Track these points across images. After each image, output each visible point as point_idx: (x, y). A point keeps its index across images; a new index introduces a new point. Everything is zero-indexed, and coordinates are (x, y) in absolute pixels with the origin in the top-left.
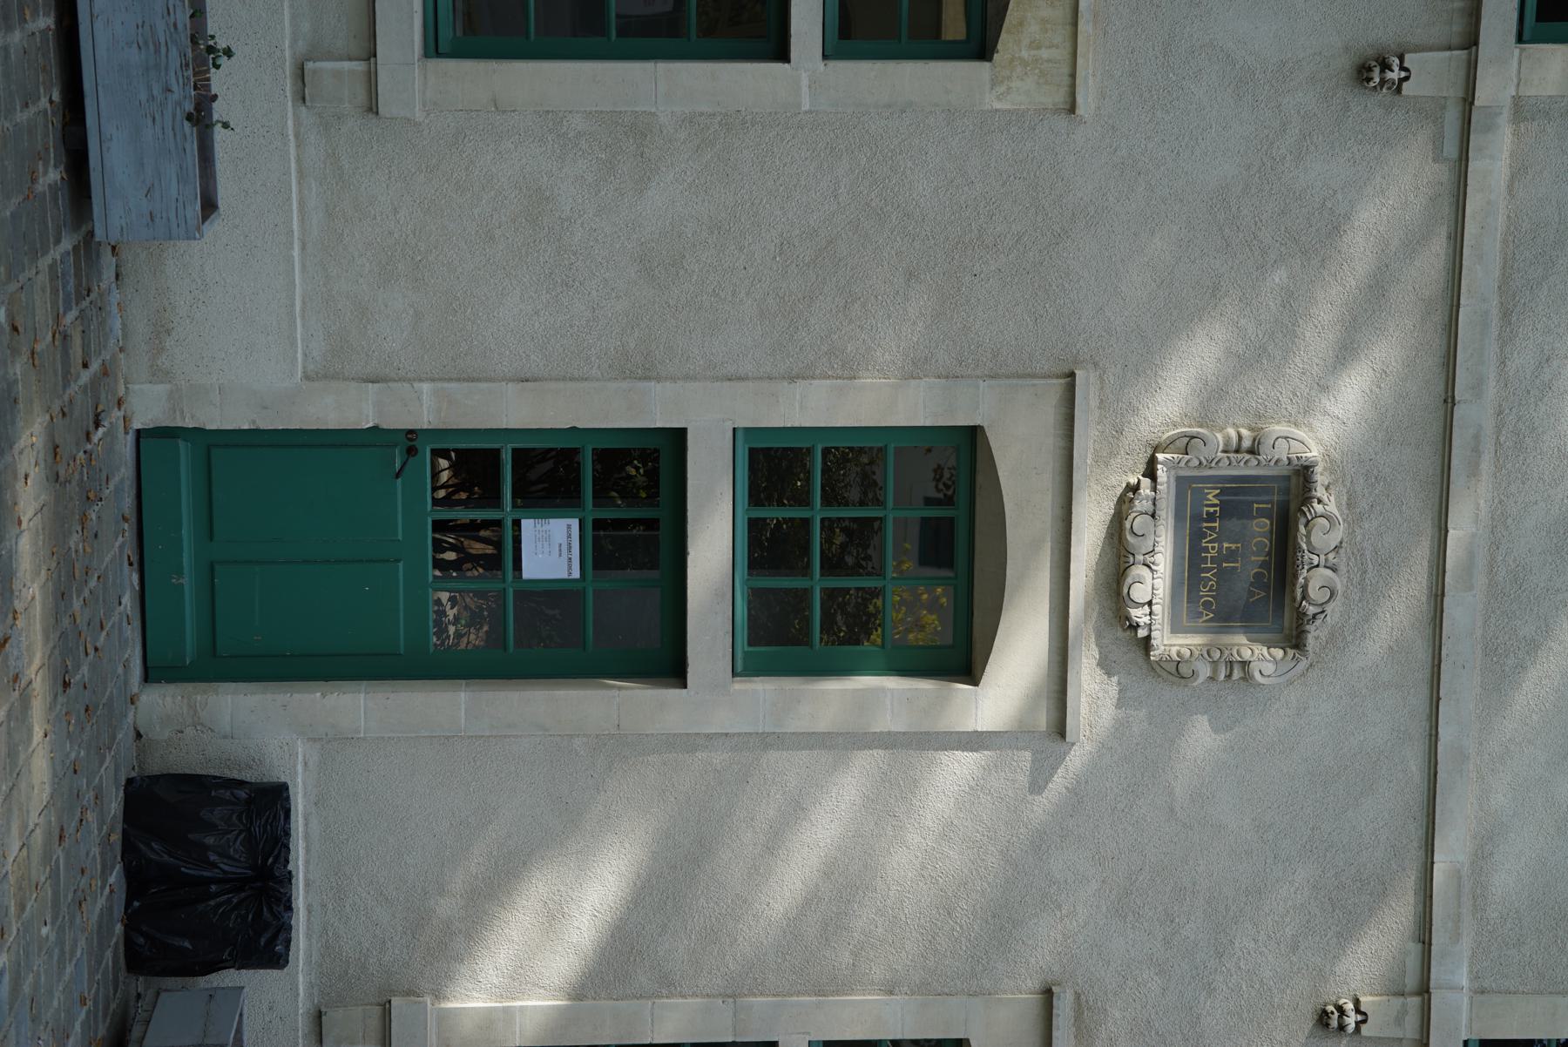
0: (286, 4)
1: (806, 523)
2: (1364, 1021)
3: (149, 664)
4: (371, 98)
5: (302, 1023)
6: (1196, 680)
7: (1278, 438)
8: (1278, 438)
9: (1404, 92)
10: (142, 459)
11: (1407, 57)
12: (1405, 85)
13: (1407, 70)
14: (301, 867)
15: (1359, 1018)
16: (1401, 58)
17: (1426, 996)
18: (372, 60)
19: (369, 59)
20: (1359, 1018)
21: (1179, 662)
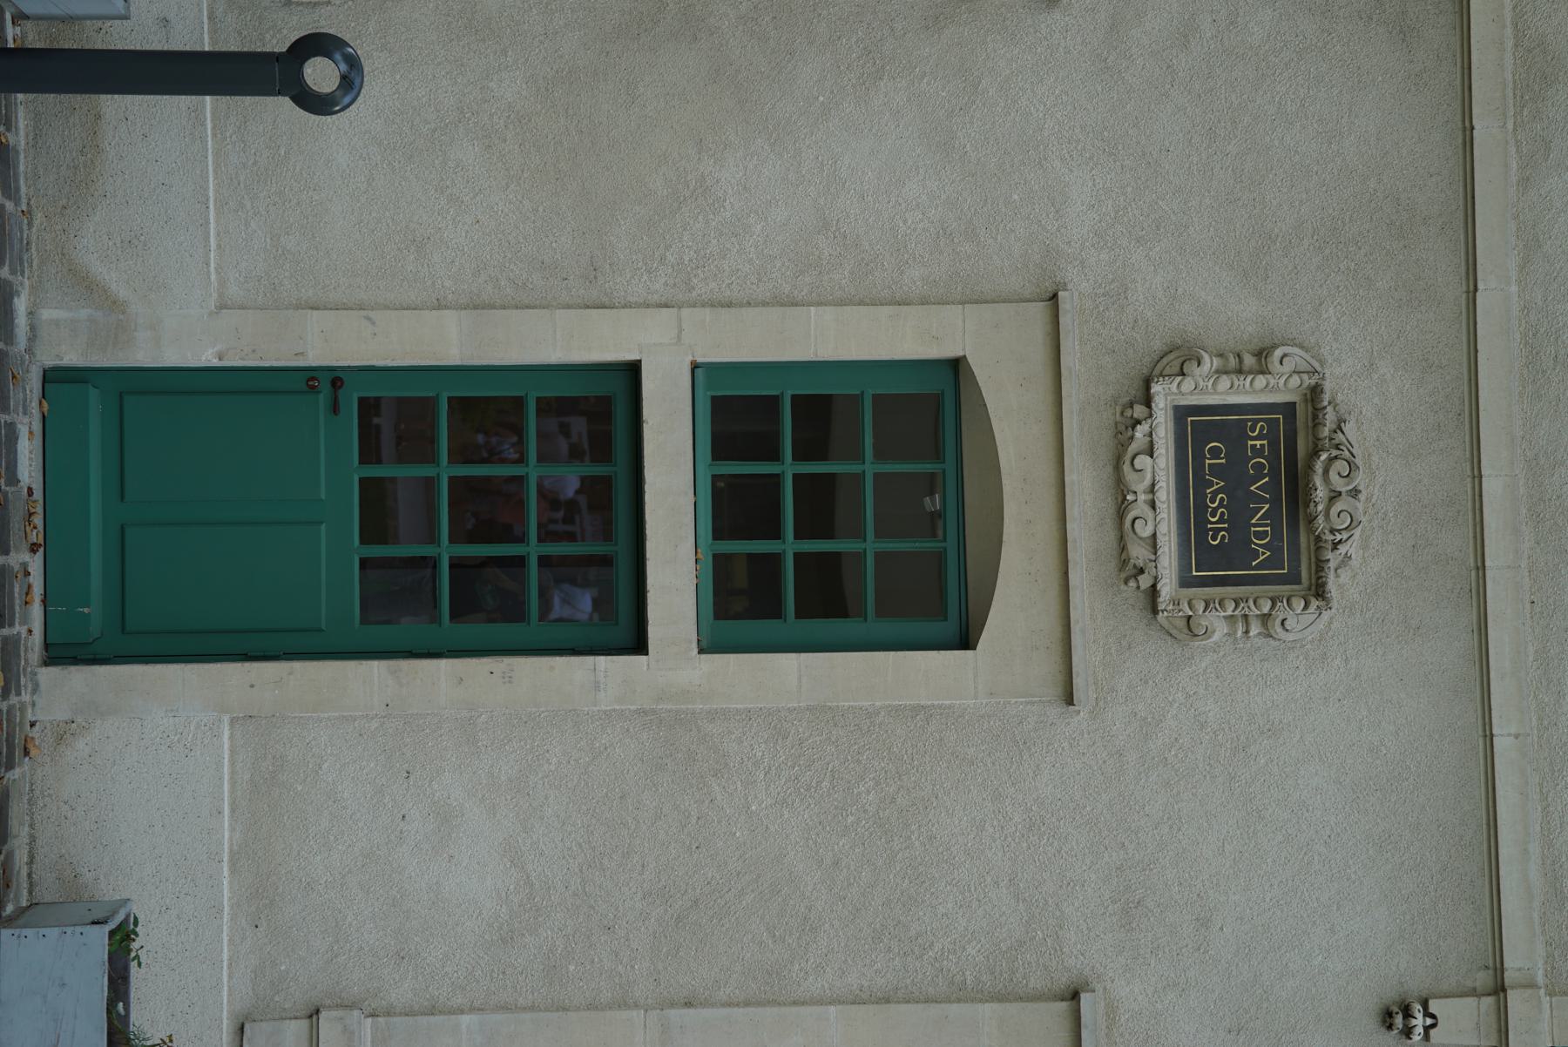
0: (205, 2)
1: (776, 480)
2: (1433, 1026)
3: (47, 378)
4: (312, 1036)
5: (227, 1026)
6: (1210, 637)
7: (1182, 365)
8: (1182, 365)
9: (1433, 1040)
10: (47, 508)
11: (1431, 1002)
12: (1432, 1032)
13: (1433, 1016)
14: (212, 221)
15: (1429, 1021)
16: (1425, 1005)
17: (1502, 995)
18: (315, 1018)
19: (311, 1016)
20: (1429, 1021)
21: (1190, 616)
